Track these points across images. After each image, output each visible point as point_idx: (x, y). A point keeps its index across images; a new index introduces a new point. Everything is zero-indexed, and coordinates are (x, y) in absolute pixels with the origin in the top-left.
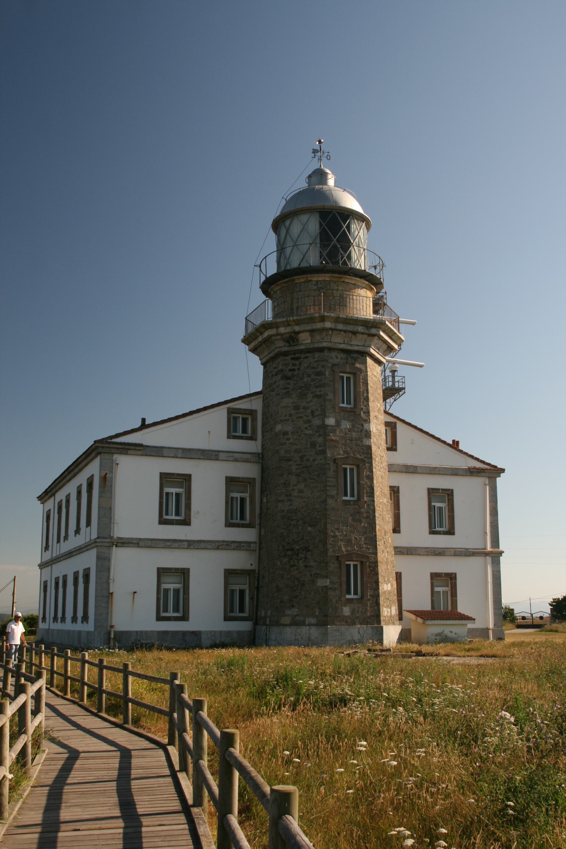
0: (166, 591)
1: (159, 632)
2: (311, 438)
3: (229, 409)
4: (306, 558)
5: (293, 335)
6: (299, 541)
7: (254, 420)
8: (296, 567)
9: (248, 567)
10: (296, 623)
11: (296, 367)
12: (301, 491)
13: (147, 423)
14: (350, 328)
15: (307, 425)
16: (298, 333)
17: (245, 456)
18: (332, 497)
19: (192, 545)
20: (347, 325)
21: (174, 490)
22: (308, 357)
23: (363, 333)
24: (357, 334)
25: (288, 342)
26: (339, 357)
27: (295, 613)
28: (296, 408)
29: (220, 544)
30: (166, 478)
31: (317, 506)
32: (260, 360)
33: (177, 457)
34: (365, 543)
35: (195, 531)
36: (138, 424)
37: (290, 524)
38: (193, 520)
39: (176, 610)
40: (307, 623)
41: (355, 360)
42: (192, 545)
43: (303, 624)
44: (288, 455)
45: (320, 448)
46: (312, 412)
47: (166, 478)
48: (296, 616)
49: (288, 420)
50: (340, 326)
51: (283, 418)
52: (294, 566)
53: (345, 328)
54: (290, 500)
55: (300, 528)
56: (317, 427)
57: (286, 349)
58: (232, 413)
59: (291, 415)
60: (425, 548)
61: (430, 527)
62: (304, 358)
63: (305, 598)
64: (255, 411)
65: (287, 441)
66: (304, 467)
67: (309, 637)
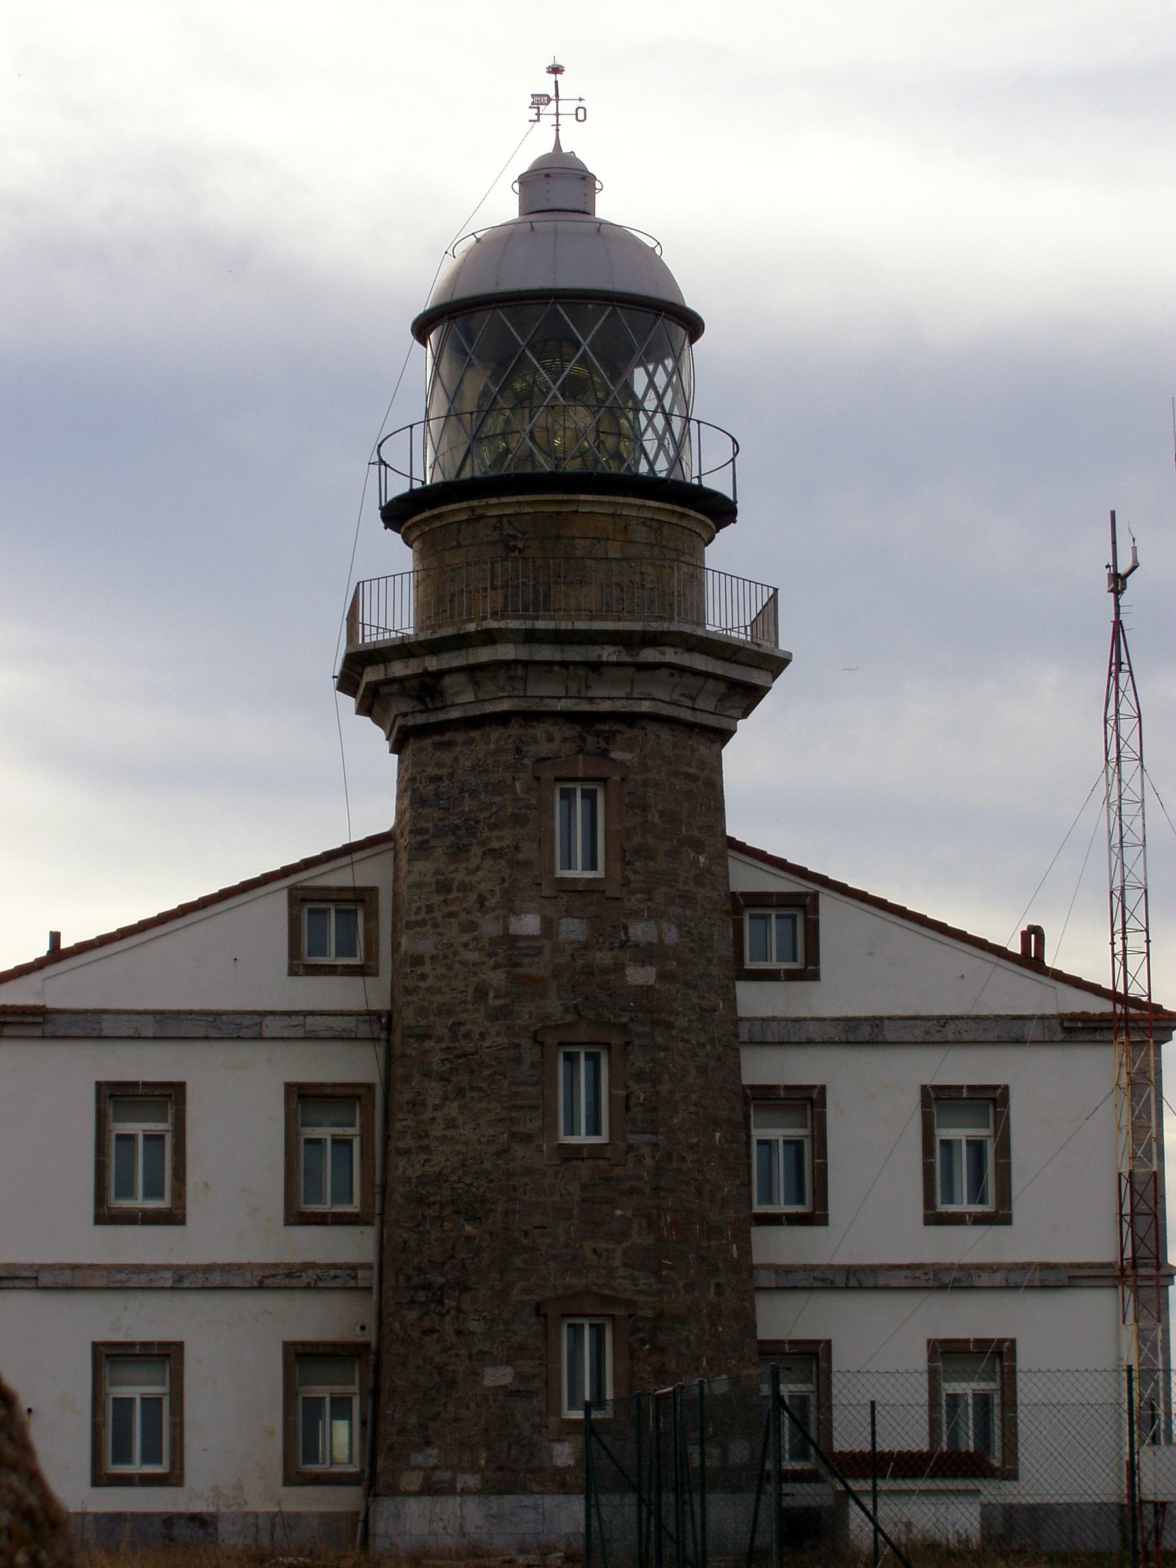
0: (124, 1405)
1: (97, 1517)
2: (475, 974)
3: (292, 890)
4: (459, 1310)
5: (428, 680)
6: (443, 1264)
7: (372, 916)
8: (435, 1336)
9: (358, 1337)
10: (429, 1489)
11: (444, 772)
12: (451, 1124)
13: (65, 944)
14: (574, 654)
15: (466, 937)
16: (440, 674)
17: (350, 1023)
18: (527, 1138)
19: (185, 1280)
20: (566, 648)
21: (138, 1128)
22: (472, 741)
23: (618, 664)
24: (603, 669)
25: (421, 699)
26: (557, 736)
27: (432, 1462)
28: (444, 887)
29: (267, 1273)
30: (115, 1097)
31: (487, 1165)
32: (725, 735)
33: (140, 1038)
34: (625, 1265)
35: (204, 1239)
36: (42, 949)
37: (424, 1217)
38: (191, 1210)
39: (151, 1455)
40: (459, 1486)
41: (607, 740)
42: (185, 1280)
43: (448, 1489)
44: (423, 1023)
45: (499, 1002)
46: (481, 900)
47: (115, 1097)
48: (436, 1468)
49: (423, 923)
50: (545, 653)
51: (413, 918)
52: (432, 1331)
53: (558, 657)
54: (425, 1149)
55: (447, 1225)
56: (492, 941)
57: (420, 719)
58: (304, 900)
59: (430, 909)
60: (909, 1267)
61: (929, 1202)
62: (465, 743)
63: (455, 1420)
64: (373, 891)
65: (422, 984)
66: (459, 1057)
67: (461, 1526)
